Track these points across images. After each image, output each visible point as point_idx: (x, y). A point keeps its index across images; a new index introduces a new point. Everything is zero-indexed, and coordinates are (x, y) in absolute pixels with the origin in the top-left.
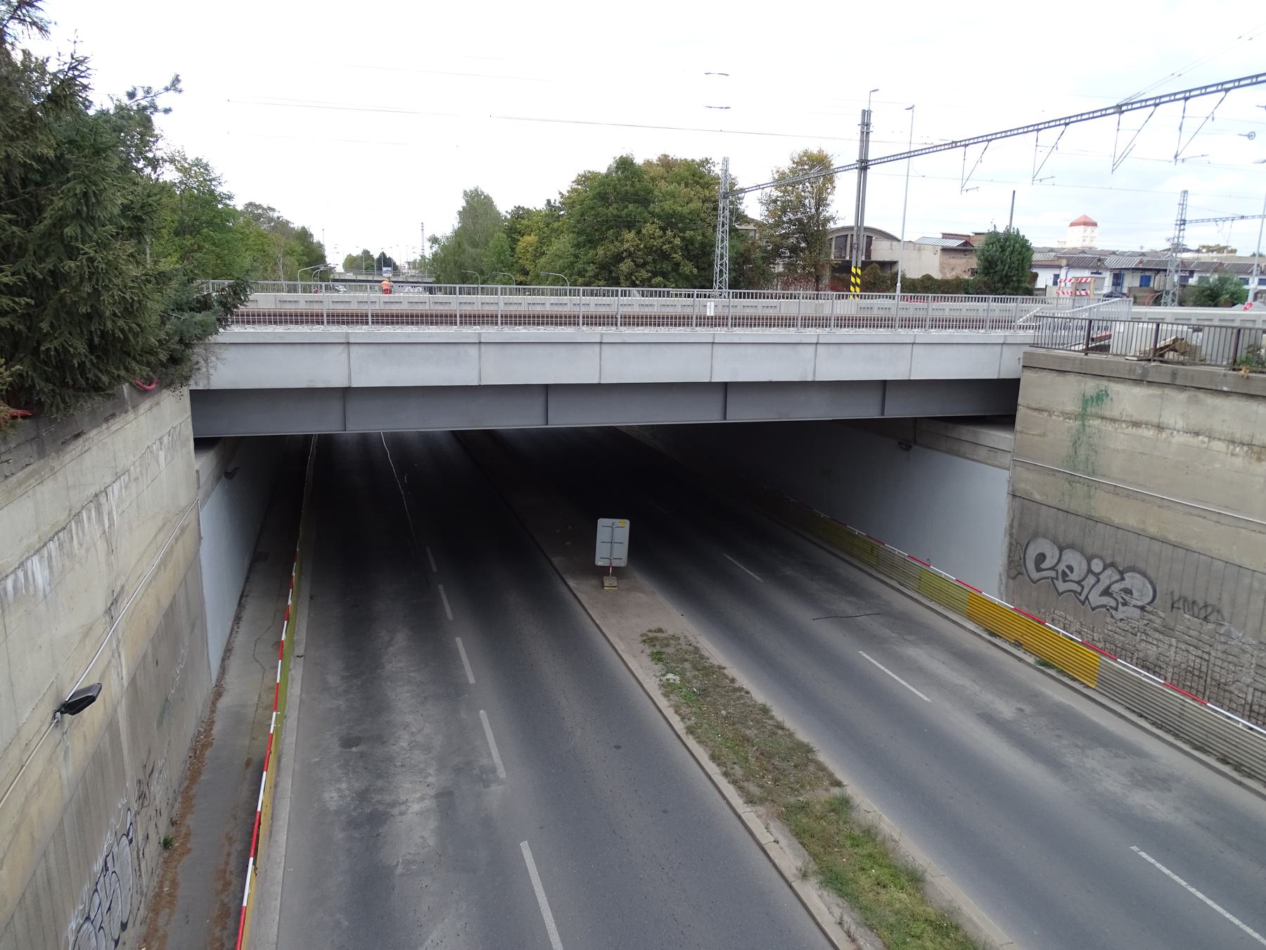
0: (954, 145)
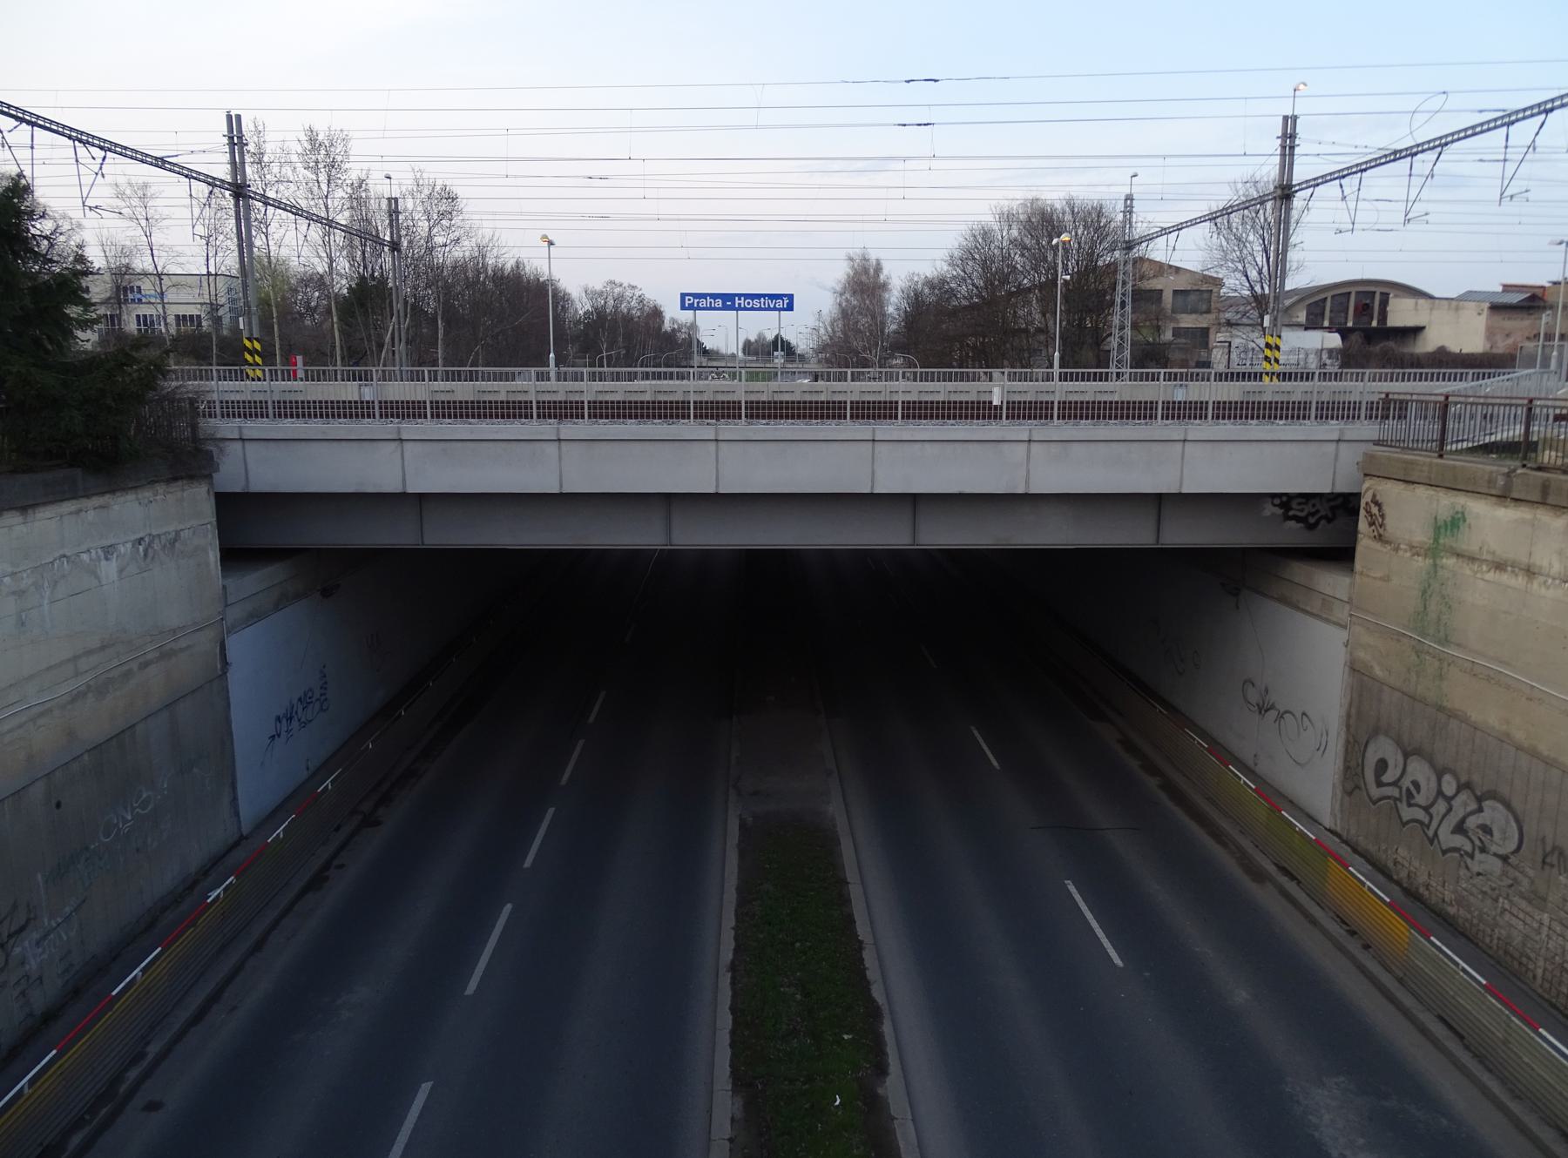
0: (1396, 156)
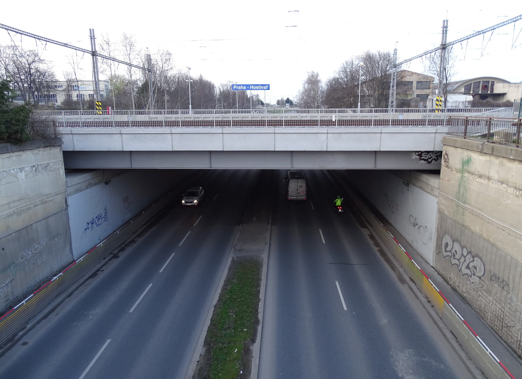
0: (479, 33)
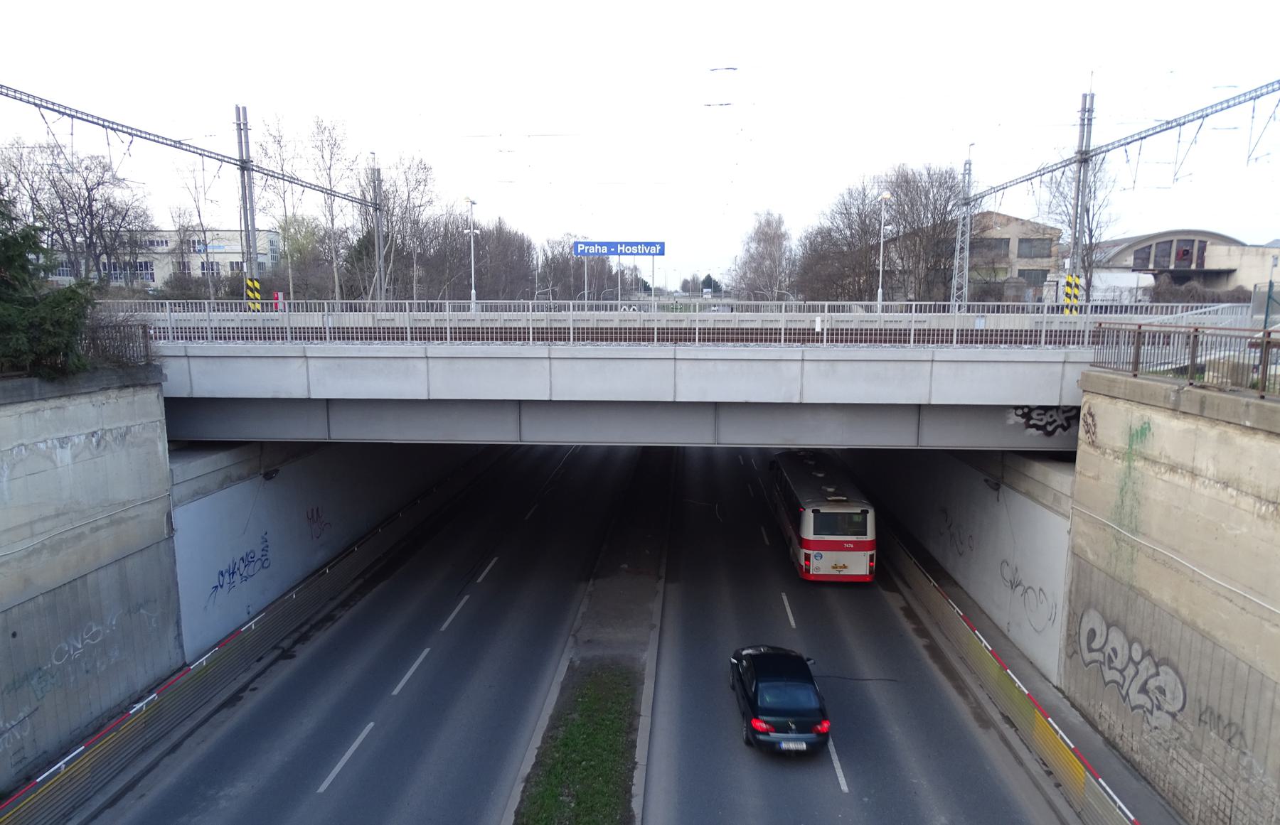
0: (1169, 126)
